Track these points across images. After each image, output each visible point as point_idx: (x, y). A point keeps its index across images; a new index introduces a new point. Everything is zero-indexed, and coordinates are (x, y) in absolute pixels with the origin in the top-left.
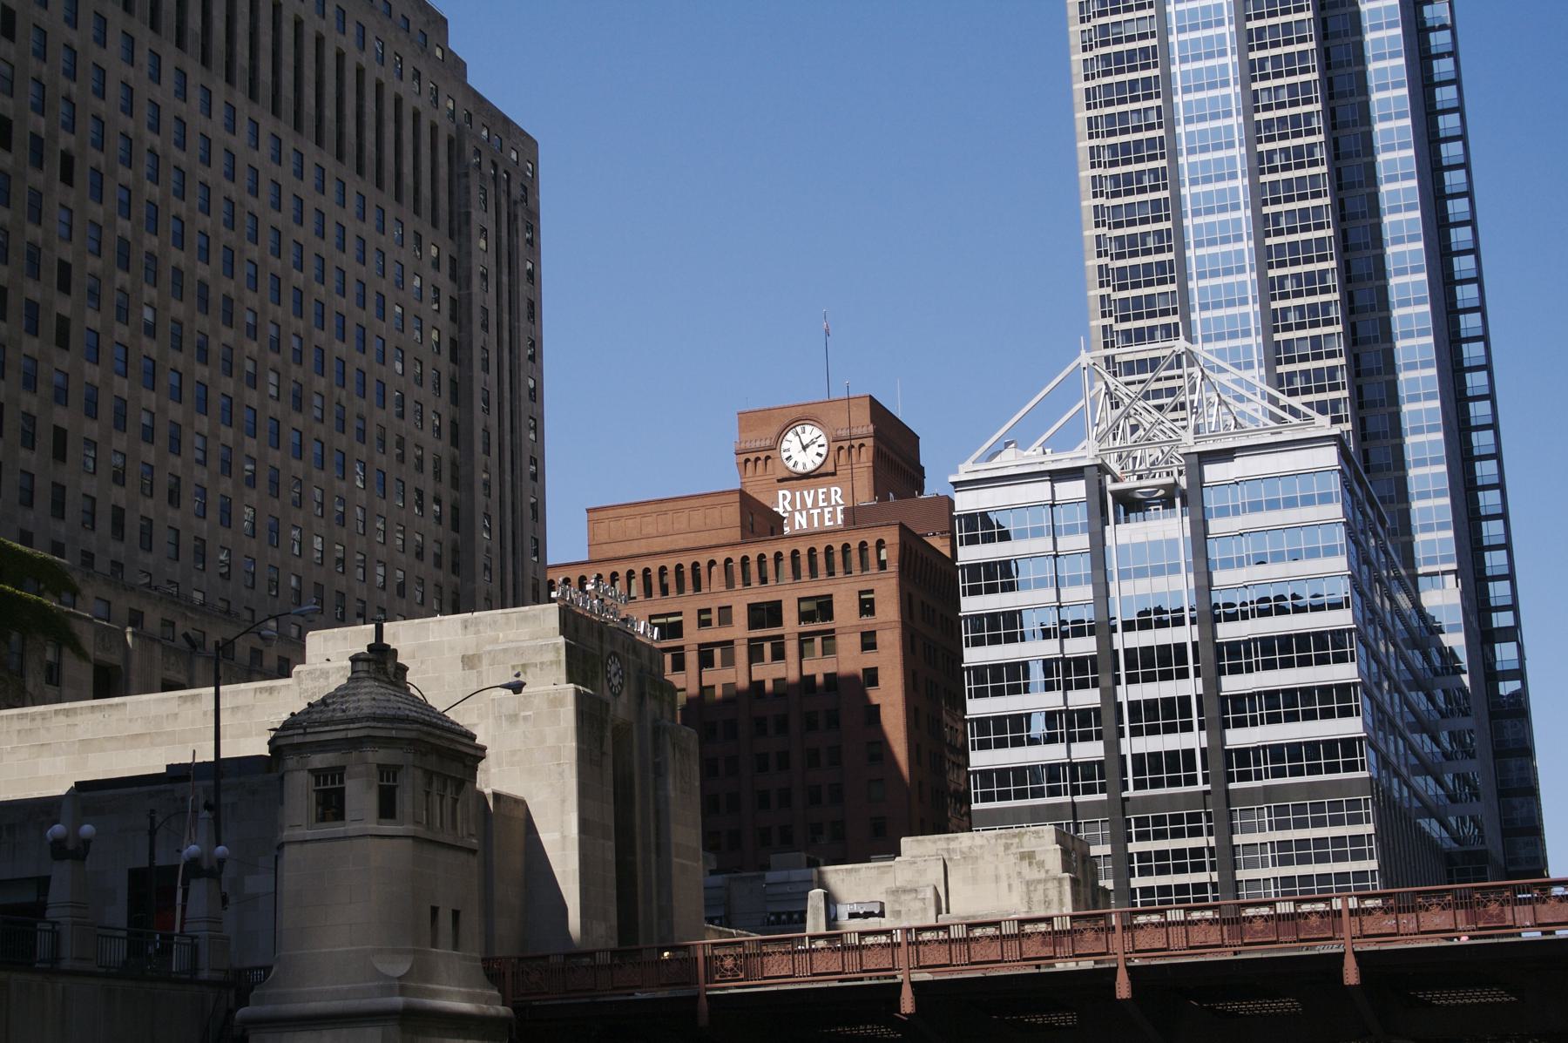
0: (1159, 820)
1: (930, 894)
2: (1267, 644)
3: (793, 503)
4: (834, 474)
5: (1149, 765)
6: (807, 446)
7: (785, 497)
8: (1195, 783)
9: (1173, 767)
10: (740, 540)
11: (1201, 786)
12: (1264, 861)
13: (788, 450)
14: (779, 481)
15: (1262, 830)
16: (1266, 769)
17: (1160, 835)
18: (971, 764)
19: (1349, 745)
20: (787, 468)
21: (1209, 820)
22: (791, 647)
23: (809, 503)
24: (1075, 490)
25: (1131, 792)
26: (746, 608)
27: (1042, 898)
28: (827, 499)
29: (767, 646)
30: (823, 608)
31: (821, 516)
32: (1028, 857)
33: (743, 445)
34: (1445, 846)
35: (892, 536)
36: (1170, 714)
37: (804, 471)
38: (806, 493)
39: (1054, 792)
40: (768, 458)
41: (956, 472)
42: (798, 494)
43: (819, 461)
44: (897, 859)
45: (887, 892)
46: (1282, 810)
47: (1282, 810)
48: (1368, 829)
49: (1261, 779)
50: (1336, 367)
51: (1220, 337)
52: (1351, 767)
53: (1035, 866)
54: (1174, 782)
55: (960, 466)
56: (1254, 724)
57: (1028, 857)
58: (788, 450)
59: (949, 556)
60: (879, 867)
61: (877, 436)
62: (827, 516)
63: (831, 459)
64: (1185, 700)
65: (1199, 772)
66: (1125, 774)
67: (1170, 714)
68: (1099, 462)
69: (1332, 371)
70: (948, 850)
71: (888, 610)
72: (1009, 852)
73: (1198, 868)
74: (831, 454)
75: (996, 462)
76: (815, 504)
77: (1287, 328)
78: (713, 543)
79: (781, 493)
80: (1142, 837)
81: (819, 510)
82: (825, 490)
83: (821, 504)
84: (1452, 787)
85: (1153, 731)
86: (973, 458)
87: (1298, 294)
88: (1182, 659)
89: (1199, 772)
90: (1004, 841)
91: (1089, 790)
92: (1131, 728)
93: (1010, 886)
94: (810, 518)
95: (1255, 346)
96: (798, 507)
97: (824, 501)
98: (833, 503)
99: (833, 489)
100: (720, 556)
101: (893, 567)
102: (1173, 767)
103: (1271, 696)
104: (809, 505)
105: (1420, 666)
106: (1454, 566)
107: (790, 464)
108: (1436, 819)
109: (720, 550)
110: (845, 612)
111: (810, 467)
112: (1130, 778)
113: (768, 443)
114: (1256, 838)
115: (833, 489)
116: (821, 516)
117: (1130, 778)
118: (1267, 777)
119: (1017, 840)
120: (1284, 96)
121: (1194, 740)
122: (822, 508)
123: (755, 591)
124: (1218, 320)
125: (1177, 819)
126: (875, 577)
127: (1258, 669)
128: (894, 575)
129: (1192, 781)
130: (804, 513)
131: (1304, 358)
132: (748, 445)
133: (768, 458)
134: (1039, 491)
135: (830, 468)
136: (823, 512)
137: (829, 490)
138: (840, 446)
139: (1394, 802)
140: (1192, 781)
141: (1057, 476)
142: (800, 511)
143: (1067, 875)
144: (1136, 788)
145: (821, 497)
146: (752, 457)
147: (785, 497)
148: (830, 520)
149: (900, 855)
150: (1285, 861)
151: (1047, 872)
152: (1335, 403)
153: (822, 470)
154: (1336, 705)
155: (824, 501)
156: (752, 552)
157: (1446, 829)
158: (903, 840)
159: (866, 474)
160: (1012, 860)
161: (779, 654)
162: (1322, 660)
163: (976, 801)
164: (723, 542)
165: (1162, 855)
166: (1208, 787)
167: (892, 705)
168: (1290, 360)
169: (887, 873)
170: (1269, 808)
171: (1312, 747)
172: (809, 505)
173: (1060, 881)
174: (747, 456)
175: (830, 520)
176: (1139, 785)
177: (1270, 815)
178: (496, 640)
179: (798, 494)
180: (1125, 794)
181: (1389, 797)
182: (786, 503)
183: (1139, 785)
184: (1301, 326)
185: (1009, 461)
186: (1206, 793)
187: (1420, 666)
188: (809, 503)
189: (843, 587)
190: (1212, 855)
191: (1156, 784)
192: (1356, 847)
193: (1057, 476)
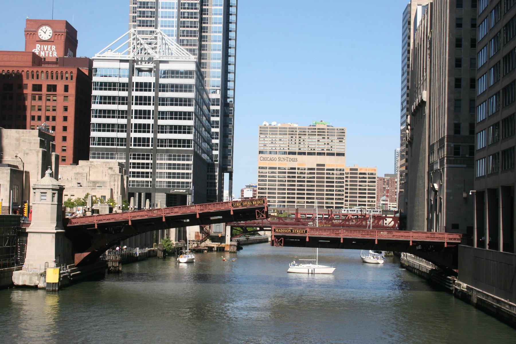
0: (139, 155)
3: (40, 48)
4: (53, 42)
5: (138, 140)
6: (46, 32)
7: (38, 46)
11: (150, 147)
13: (40, 33)
14: (37, 41)
17: (139, 159)
19: (189, 141)
20: (39, 38)
21: (152, 156)
22: (44, 98)
23: (45, 49)
24: (127, 65)
25: (132, 147)
26: (32, 85)
28: (51, 49)
30: (52, 88)
31: (49, 53)
32: (111, 168)
33: (27, 29)
35: (75, 72)
36: (144, 128)
37: (45, 40)
38: (45, 46)
39: (112, 145)
40: (34, 34)
41: (94, 56)
42: (42, 46)
43: (49, 37)
45: (74, 173)
46: (170, 156)
48: (191, 162)
52: (188, 147)
54: (144, 145)
55: (95, 54)
59: (87, 73)
60: (72, 167)
61: (67, 33)
62: (50, 54)
63: (53, 37)
64: (149, 125)
65: (150, 144)
67: (144, 128)
68: (133, 59)
69: (195, 31)
71: (72, 91)
74: (53, 36)
76: (47, 50)
78: (23, 66)
79: (37, 45)
81: (48, 52)
82: (50, 46)
83: (49, 50)
85: (140, 132)
86: (99, 53)
87: (188, 9)
89: (150, 144)
90: (105, 164)
91: (122, 145)
92: (134, 130)
93: (106, 175)
94: (45, 54)
96: (42, 50)
97: (50, 49)
99: (53, 46)
100: (26, 70)
101: (74, 79)
104: (45, 50)
105: (207, 102)
106: (219, 88)
107: (41, 37)
109: (26, 68)
111: (47, 39)
113: (34, 30)
114: (163, 162)
115: (53, 46)
116: (49, 53)
118: (167, 147)
121: (150, 135)
123: (35, 81)
124: (166, 12)
125: (143, 155)
129: (148, 146)
130: (44, 52)
131: (188, 27)
133: (34, 34)
134: (117, 65)
135: (52, 40)
136: (49, 52)
138: (55, 33)
140: (148, 146)
141: (122, 61)
142: (43, 51)
143: (120, 174)
145: (49, 48)
146: (29, 33)
147: (38, 46)
148: (51, 55)
151: (115, 173)
152: (194, 50)
154: (183, 117)
155: (50, 49)
156: (35, 70)
158: (80, 161)
159: (63, 43)
161: (40, 99)
163: (91, 145)
164: (26, 66)
165: (139, 164)
166: (152, 148)
167: (71, 117)
171: (180, 141)
172: (45, 50)
173: (118, 175)
174: (28, 33)
175: (51, 55)
176: (135, 145)
177: (167, 157)
179: (42, 46)
180: (130, 147)
182: (39, 48)
183: (135, 145)
184: (188, 18)
185: (109, 54)
186: (151, 149)
187: (207, 114)
188: (45, 49)
189: (60, 83)
190: (151, 165)
191: (139, 145)
193: (122, 61)
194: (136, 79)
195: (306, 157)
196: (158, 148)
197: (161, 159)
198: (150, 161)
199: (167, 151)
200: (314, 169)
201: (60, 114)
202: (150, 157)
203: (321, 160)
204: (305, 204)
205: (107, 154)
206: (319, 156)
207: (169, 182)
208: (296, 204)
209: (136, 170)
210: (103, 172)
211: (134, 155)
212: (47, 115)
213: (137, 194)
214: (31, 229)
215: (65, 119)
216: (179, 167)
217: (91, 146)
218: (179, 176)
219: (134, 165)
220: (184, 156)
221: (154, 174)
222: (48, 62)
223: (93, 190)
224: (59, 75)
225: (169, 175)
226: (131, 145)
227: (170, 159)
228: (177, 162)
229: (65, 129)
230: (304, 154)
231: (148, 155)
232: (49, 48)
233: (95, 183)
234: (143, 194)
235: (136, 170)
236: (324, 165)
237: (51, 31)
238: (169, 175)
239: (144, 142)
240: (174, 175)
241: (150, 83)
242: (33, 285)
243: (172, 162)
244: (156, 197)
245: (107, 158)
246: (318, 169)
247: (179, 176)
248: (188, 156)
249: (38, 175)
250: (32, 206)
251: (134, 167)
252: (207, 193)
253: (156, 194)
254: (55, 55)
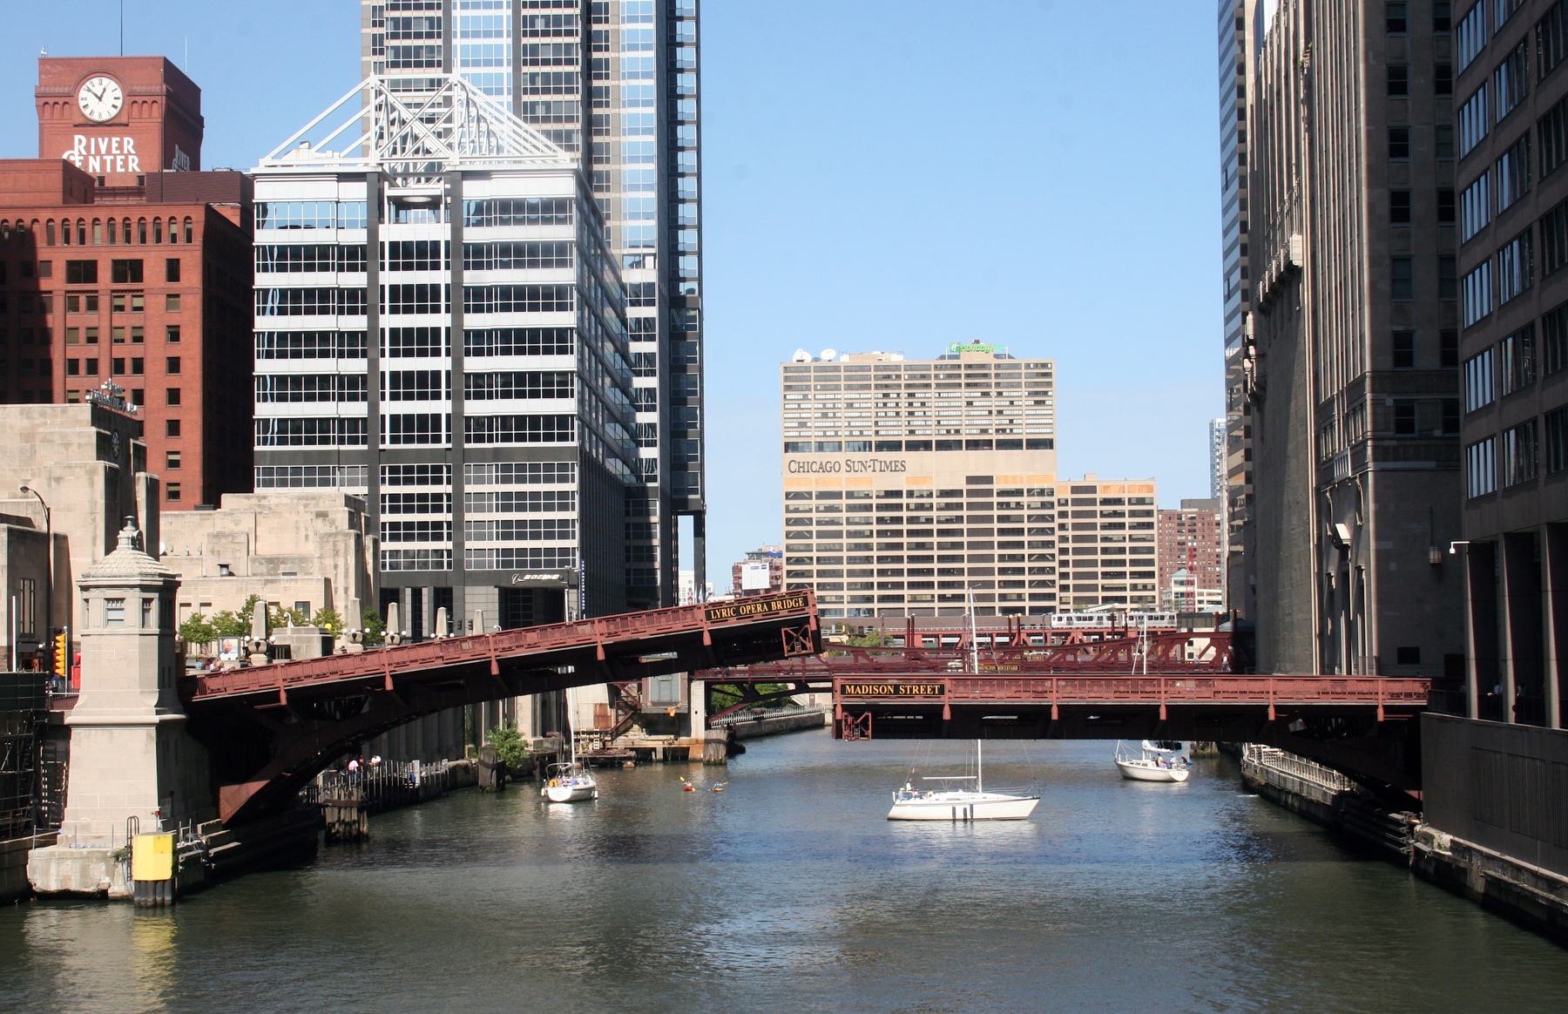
0: (409, 470)
1: (243, 539)
2: (505, 291)
3: (88, 148)
5: (405, 426)
6: (102, 95)
7: (80, 141)
8: (440, 441)
10: (61, 204)
11: (444, 445)
12: (490, 478)
13: (86, 99)
14: (75, 126)
15: (490, 482)
16: (497, 435)
19: (563, 420)
20: (83, 115)
21: (449, 471)
22: (104, 302)
23: (103, 151)
25: (388, 446)
26: (64, 264)
28: (120, 147)
29: (83, 299)
30: (129, 271)
31: (114, 163)
32: (322, 515)
33: (42, 89)
35: (198, 216)
36: (424, 385)
37: (100, 120)
38: (100, 140)
39: (325, 441)
41: (257, 165)
42: (93, 140)
43: (114, 112)
46: (507, 468)
47: (507, 468)
48: (573, 487)
50: (572, 131)
51: (476, 63)
52: (563, 437)
54: (423, 440)
55: (261, 160)
56: (490, 397)
57: (322, 515)
58: (86, 99)
59: (236, 221)
62: (119, 163)
65: (444, 433)
67: (424, 385)
71: (192, 276)
73: (438, 509)
75: (286, 160)
76: (109, 152)
77: (534, 34)
79: (77, 137)
80: (394, 482)
81: (112, 157)
82: (118, 139)
83: (114, 151)
88: (436, 340)
89: (444, 433)
91: (354, 441)
93: (307, 536)
94: (103, 163)
95: (505, 48)
96: (93, 152)
97: (117, 149)
98: (126, 152)
99: (126, 139)
100: (44, 216)
103: (506, 334)
110: (154, 272)
111: (105, 117)
115: (126, 139)
116: (114, 163)
118: (497, 441)
120: (540, 26)
121: (443, 407)
122: (115, 155)
123: (73, 250)
125: (423, 469)
126: (182, 248)
127: (496, 311)
128: (198, 248)
129: (437, 439)
130: (98, 158)
131: (546, 62)
132: (47, 90)
135: (124, 120)
136: (115, 159)
137: (122, 141)
138: (132, 99)
140: (437, 439)
142: (94, 156)
144: (391, 442)
145: (115, 145)
146: (51, 101)
147: (80, 141)
150: (507, 508)
151: (336, 528)
152: (569, 134)
153: (116, 121)
155: (117, 149)
156: (73, 215)
160: (310, 516)
161: (93, 305)
162: (548, 351)
163: (259, 444)
166: (450, 446)
167: (191, 359)
168: (534, 63)
170: (497, 465)
171: (534, 419)
174: (46, 100)
175: (122, 167)
176: (394, 440)
177: (497, 471)
179: (93, 140)
180: (381, 447)
182: (82, 147)
183: (394, 440)
184: (545, 34)
186: (447, 449)
188: (103, 151)
189: (153, 254)
191: (409, 440)
194: (390, 233)
195: (933, 455)
196: (467, 446)
197: (479, 481)
198: (445, 488)
200: (958, 493)
201: (156, 350)
203: (978, 463)
204: (936, 605)
206: (973, 453)
208: (906, 605)
211: (394, 470)
212: (116, 355)
213: (408, 591)
214: (77, 714)
215: (174, 365)
217: (257, 448)
222: (114, 189)
223: (269, 585)
224: (150, 230)
225: (506, 530)
226: (383, 441)
229: (174, 396)
230: (926, 445)
231: (438, 469)
232: (115, 145)
233: (274, 562)
234: (425, 591)
236: (989, 480)
237: (119, 93)
238: (506, 530)
239: (423, 427)
241: (436, 244)
242: (91, 889)
243: (514, 488)
244: (468, 598)
245: (310, 483)
246: (971, 493)
249: (94, 544)
250: (79, 644)
252: (628, 581)
253: (468, 589)
254: (134, 165)
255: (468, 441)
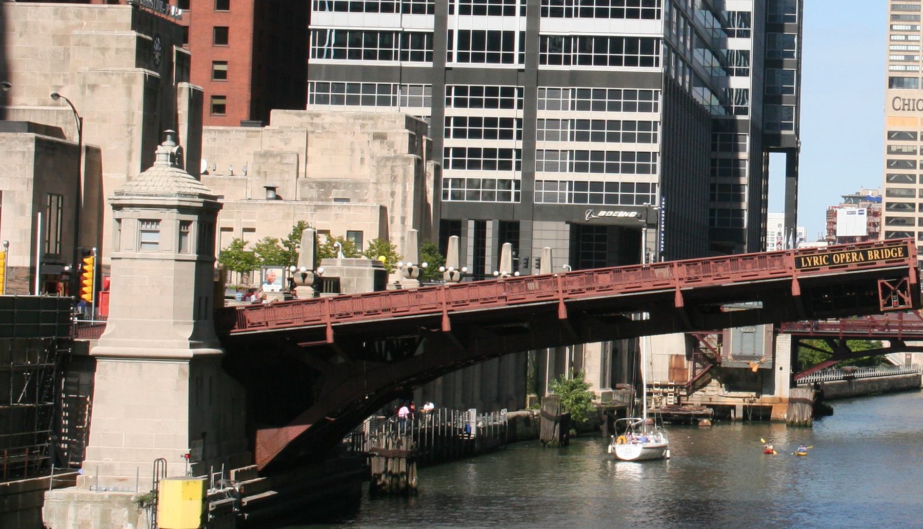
9: (494, 45)
11: (516, 65)
12: (564, 134)
16: (575, 56)
18: (311, 23)
19: (648, 44)
21: (520, 95)
25: (455, 64)
27: (390, 173)
32: (380, 137)
34: (714, 113)
44: (267, 127)
46: (584, 93)
48: (655, 116)
49: (570, 64)
52: (647, 62)
53: (385, 145)
54: (493, 59)
57: (380, 137)
60: (248, 131)
65: (516, 52)
66: (451, 47)
70: (312, 124)
72: (364, 131)
80: (460, 103)
84: (727, 19)
89: (516, 52)
90: (361, 121)
91: (418, 57)
93: (362, 160)
102: (494, 45)
108: (710, 50)
112: (455, 51)
117: (455, 51)
118: (575, 63)
119: (372, 122)
125: (492, 91)
129: (509, 59)
139: (678, 88)
140: (509, 59)
149: (268, 124)
151: (395, 152)
157: (719, 20)
160: (367, 138)
163: (314, 57)
166: (523, 66)
169: (255, 137)
170: (573, 90)
171: (617, 42)
173: (408, 159)
176: (462, 58)
178: (452, 274)
180: (448, 65)
181: (674, 85)
183: (462, 58)
190: (519, 125)
191: (478, 58)
192: (644, 131)
196: (541, 67)
197: (553, 106)
198: (515, 113)
199: (574, 77)
202: (516, 98)
205: (369, 88)
207: (581, 185)
209: (467, 143)
210: (353, 150)
211: (461, 91)
213: (471, 224)
216: (613, 131)
217: (311, 61)
218: (613, 162)
219: (462, 127)
220: (630, 94)
221: (527, 157)
223: (319, 212)
225: (581, 161)
226: (450, 58)
227: (583, 106)
228: (622, 116)
231: (508, 92)
233: (325, 186)
234: (489, 225)
235: (467, 143)
238: (581, 161)
240: (597, 161)
243: (591, 115)
244: (536, 235)
245: (368, 101)
247: (613, 162)
248: (646, 95)
250: (108, 267)
251: (459, 134)
252: (712, 222)
253: (537, 224)
255: (543, 61)
